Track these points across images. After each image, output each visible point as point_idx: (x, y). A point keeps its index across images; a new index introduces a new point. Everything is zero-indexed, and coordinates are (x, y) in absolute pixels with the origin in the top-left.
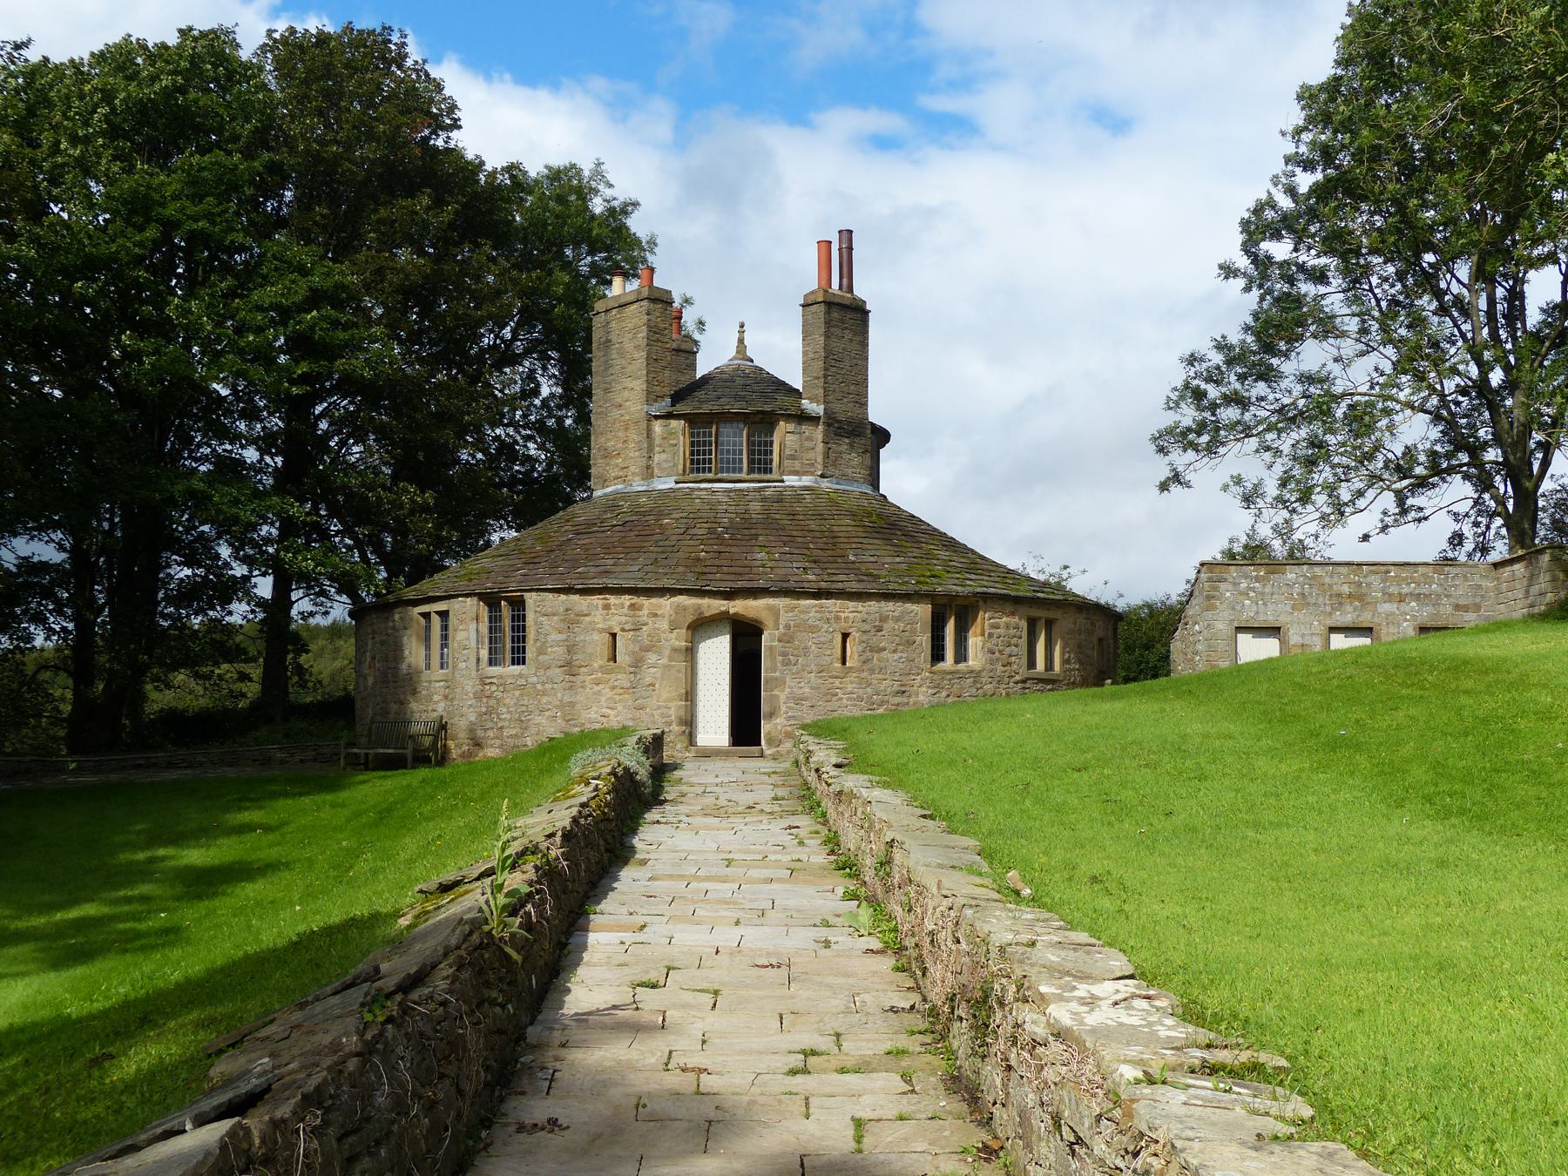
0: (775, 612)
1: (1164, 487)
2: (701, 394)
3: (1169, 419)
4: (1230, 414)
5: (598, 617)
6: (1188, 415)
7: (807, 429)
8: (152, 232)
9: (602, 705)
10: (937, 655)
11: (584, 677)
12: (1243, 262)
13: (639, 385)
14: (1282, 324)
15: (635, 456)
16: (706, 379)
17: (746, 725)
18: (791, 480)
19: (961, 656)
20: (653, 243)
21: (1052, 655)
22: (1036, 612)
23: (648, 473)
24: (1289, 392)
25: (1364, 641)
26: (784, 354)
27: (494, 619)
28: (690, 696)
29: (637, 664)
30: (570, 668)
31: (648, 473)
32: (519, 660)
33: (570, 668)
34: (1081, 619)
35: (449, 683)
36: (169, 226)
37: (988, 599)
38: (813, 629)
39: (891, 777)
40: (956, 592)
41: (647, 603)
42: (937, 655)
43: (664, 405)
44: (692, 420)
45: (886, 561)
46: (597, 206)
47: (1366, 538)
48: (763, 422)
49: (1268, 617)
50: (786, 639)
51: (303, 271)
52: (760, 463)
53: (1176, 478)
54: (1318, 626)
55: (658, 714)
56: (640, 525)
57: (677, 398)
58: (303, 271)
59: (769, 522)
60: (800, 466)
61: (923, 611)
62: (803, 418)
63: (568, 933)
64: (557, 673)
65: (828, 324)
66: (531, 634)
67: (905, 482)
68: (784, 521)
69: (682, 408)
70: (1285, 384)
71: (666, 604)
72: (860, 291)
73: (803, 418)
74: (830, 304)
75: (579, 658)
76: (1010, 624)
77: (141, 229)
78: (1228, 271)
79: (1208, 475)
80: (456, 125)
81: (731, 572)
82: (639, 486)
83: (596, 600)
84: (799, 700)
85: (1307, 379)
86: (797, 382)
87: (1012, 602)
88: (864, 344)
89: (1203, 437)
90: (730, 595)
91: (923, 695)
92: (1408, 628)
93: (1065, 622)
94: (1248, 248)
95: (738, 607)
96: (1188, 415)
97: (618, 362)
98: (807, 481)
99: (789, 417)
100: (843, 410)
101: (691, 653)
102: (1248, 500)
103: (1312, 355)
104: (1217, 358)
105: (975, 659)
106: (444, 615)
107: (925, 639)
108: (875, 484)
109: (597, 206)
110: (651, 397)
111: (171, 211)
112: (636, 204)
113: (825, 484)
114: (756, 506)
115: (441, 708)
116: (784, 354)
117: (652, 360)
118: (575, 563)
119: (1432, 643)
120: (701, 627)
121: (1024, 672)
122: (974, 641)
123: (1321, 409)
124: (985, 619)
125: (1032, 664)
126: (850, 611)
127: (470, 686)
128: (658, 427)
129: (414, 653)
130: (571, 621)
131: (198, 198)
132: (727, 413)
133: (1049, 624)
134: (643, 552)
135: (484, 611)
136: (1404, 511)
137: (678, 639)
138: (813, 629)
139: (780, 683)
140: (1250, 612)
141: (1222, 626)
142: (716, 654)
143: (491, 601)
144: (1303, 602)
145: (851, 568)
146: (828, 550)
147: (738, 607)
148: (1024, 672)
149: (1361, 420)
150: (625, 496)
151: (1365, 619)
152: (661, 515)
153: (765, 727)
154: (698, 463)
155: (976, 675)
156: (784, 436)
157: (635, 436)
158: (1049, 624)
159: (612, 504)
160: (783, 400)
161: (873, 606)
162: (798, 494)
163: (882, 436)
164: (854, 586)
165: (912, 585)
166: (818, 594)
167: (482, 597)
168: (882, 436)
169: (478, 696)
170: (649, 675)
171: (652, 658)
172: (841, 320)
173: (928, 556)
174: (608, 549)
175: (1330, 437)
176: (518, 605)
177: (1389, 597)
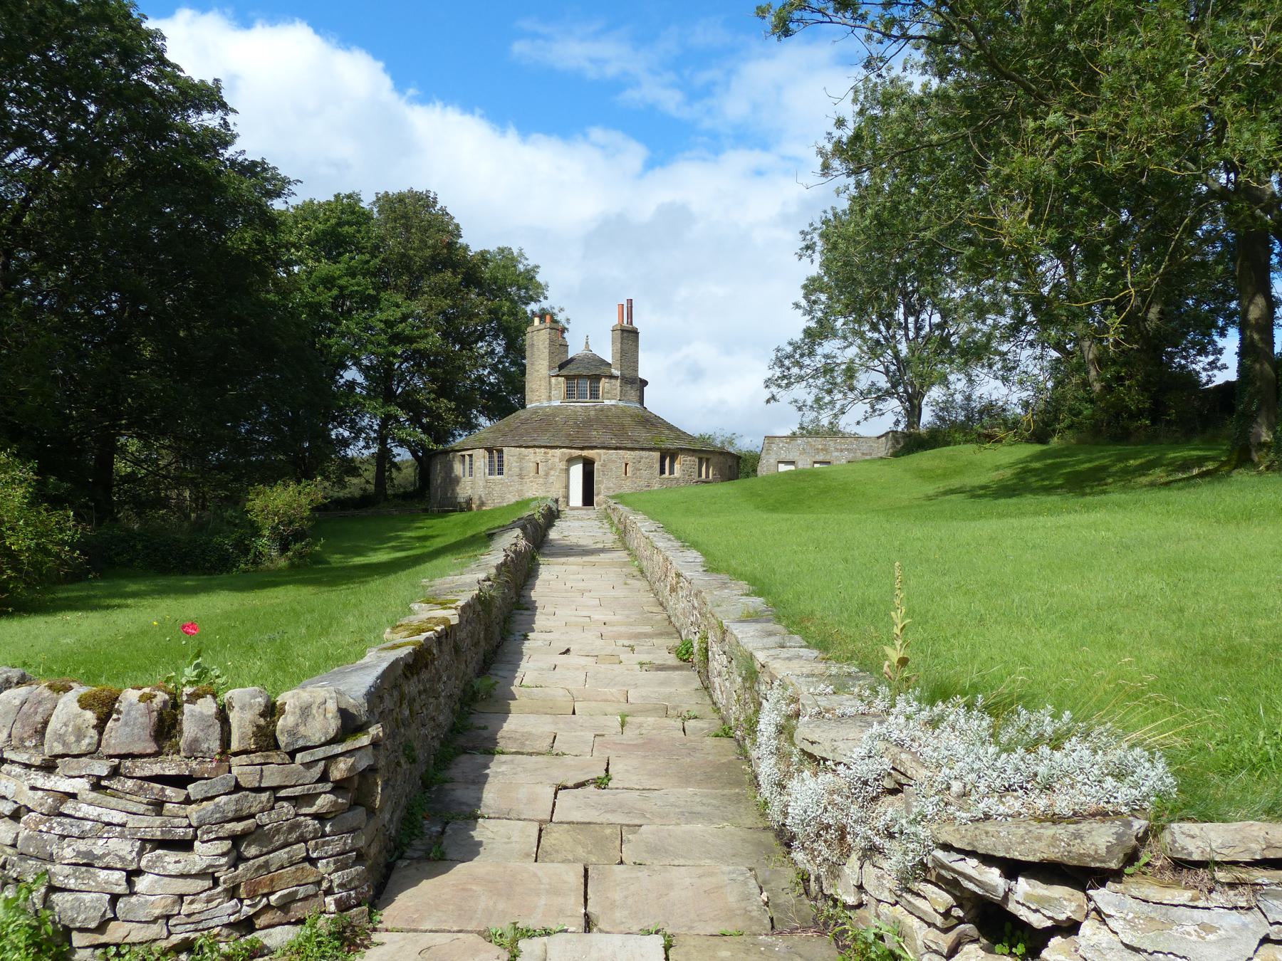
0: (599, 455)
1: (768, 401)
2: (570, 366)
3: (769, 374)
4: (795, 370)
5: (532, 456)
6: (778, 372)
7: (613, 381)
8: (335, 292)
9: (533, 490)
10: (662, 472)
11: (526, 480)
12: (804, 303)
13: (546, 363)
14: (814, 336)
15: (544, 391)
16: (572, 360)
17: (588, 499)
18: (607, 402)
19: (671, 472)
20: (547, 286)
21: (709, 472)
22: (705, 456)
23: (549, 399)
24: (818, 361)
25: (792, 468)
26: (606, 351)
27: (491, 457)
28: (567, 487)
29: (547, 475)
30: (521, 476)
31: (549, 399)
32: (501, 473)
33: (521, 476)
34: (721, 458)
35: (473, 482)
36: (342, 288)
37: (682, 450)
38: (614, 462)
39: (627, 504)
40: (669, 446)
41: (551, 452)
42: (662, 472)
43: (556, 371)
44: (567, 378)
45: (643, 435)
46: (521, 267)
47: (858, 423)
48: (597, 378)
49: (790, 458)
50: (604, 465)
51: (398, 306)
52: (595, 395)
53: (773, 398)
54: (809, 461)
55: (556, 491)
56: (546, 420)
57: (561, 367)
58: (398, 306)
59: (597, 420)
60: (611, 396)
61: (657, 455)
62: (612, 377)
63: (443, 760)
64: (516, 478)
65: (622, 338)
66: (505, 463)
67: (654, 401)
68: (603, 419)
69: (564, 372)
70: (818, 358)
71: (558, 452)
72: (635, 324)
73: (612, 377)
74: (623, 331)
75: (524, 472)
76: (691, 460)
77: (330, 290)
78: (797, 306)
79: (784, 396)
80: (452, 218)
81: (581, 441)
82: (545, 404)
83: (531, 450)
84: (608, 489)
85: (826, 356)
86: (610, 361)
87: (692, 452)
88: (637, 346)
89: (785, 381)
90: (582, 449)
91: (656, 487)
92: (844, 461)
93: (714, 459)
94: (806, 297)
95: (585, 453)
96: (778, 372)
97: (537, 353)
98: (613, 402)
99: (606, 377)
100: (628, 373)
101: (567, 470)
102: (800, 409)
103: (829, 346)
104: (789, 349)
105: (677, 473)
106: (471, 456)
107: (657, 466)
108: (642, 404)
109: (521, 267)
110: (551, 368)
111: (342, 282)
112: (538, 267)
113: (621, 403)
114: (593, 413)
115: (470, 492)
116: (606, 351)
117: (551, 353)
118: (522, 435)
119: (851, 467)
120: (571, 461)
121: (697, 479)
122: (677, 466)
123: (828, 370)
124: (681, 458)
125: (700, 475)
126: (628, 455)
127: (481, 483)
128: (553, 380)
129: (458, 468)
130: (521, 458)
131: (353, 275)
132: (581, 374)
133: (708, 460)
134: (548, 432)
135: (487, 454)
136: (874, 411)
137: (563, 465)
138: (614, 462)
139: (601, 482)
140: (783, 456)
141: (772, 461)
142: (577, 471)
143: (490, 450)
144: (804, 452)
145: (629, 438)
146: (621, 431)
147: (585, 453)
148: (697, 479)
149: (850, 373)
150: (540, 408)
151: (827, 458)
152: (555, 416)
153: (596, 499)
154: (569, 394)
155: (677, 479)
156: (604, 384)
157: (544, 383)
158: (708, 460)
159: (535, 411)
160: (604, 370)
161: (637, 452)
162: (609, 408)
163: (644, 383)
164: (630, 445)
165: (652, 445)
166: (616, 449)
167: (486, 449)
168: (644, 383)
169: (485, 487)
170: (551, 479)
171: (552, 472)
172: (628, 336)
173: (661, 433)
174: (535, 430)
175: (838, 379)
176: (500, 452)
177: (837, 450)
